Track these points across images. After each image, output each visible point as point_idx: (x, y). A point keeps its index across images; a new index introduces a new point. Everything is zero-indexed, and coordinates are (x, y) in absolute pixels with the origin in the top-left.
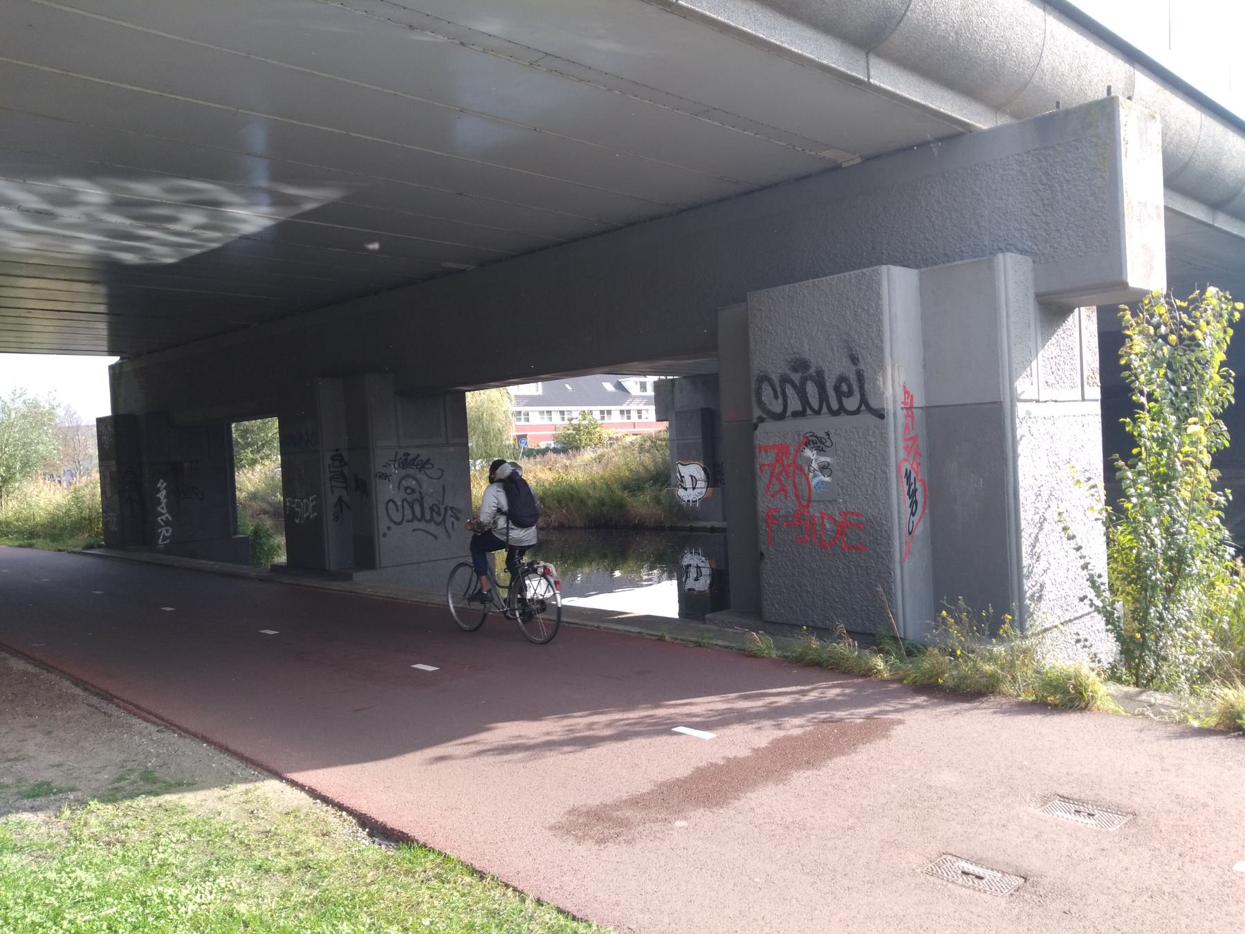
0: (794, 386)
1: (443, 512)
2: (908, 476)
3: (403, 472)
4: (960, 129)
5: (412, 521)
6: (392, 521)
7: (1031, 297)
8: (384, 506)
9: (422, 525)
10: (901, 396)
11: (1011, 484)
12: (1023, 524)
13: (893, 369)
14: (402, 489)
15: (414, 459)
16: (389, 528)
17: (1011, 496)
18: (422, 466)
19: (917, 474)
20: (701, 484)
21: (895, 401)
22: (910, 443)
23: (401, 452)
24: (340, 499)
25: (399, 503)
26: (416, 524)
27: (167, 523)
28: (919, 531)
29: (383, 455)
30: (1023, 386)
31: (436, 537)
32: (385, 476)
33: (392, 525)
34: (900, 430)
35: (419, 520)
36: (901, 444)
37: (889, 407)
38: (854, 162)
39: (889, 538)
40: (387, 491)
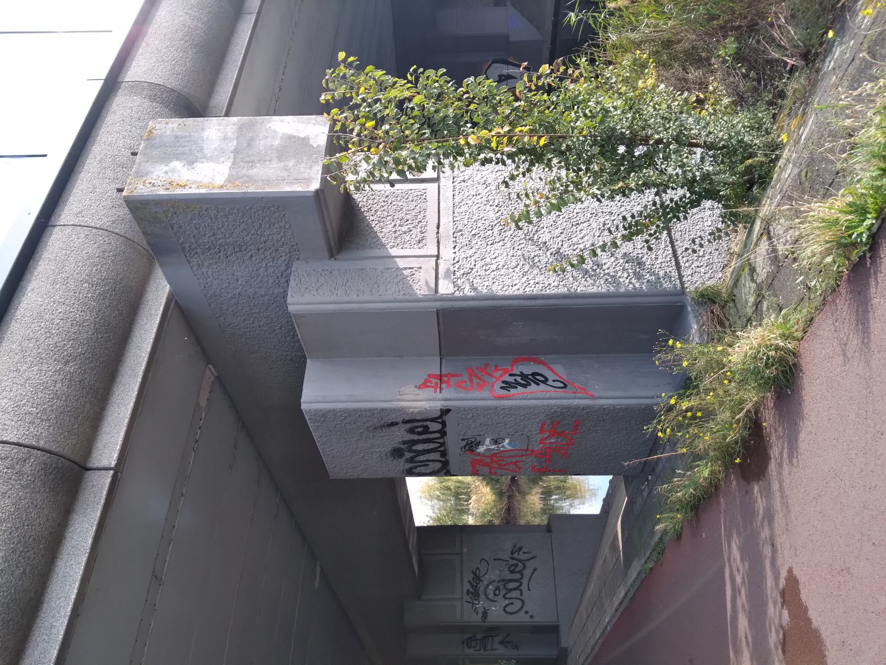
0: (416, 456)
1: (514, 562)
2: (508, 386)
3: (482, 596)
4: (173, 303)
5: (521, 591)
6: (520, 609)
7: (333, 264)
9: (525, 581)
10: (429, 393)
11: (522, 302)
12: (563, 290)
13: (402, 400)
15: (472, 585)
16: (527, 612)
17: (533, 302)
18: (478, 578)
21: (434, 400)
22: (475, 380)
23: (467, 598)
24: (501, 643)
25: (507, 602)
26: (524, 587)
28: (561, 371)
30: (421, 283)
31: (535, 570)
32: (485, 613)
33: (524, 610)
35: (521, 584)
36: (476, 394)
37: (438, 405)
38: (213, 369)
39: (569, 408)
40: (497, 613)
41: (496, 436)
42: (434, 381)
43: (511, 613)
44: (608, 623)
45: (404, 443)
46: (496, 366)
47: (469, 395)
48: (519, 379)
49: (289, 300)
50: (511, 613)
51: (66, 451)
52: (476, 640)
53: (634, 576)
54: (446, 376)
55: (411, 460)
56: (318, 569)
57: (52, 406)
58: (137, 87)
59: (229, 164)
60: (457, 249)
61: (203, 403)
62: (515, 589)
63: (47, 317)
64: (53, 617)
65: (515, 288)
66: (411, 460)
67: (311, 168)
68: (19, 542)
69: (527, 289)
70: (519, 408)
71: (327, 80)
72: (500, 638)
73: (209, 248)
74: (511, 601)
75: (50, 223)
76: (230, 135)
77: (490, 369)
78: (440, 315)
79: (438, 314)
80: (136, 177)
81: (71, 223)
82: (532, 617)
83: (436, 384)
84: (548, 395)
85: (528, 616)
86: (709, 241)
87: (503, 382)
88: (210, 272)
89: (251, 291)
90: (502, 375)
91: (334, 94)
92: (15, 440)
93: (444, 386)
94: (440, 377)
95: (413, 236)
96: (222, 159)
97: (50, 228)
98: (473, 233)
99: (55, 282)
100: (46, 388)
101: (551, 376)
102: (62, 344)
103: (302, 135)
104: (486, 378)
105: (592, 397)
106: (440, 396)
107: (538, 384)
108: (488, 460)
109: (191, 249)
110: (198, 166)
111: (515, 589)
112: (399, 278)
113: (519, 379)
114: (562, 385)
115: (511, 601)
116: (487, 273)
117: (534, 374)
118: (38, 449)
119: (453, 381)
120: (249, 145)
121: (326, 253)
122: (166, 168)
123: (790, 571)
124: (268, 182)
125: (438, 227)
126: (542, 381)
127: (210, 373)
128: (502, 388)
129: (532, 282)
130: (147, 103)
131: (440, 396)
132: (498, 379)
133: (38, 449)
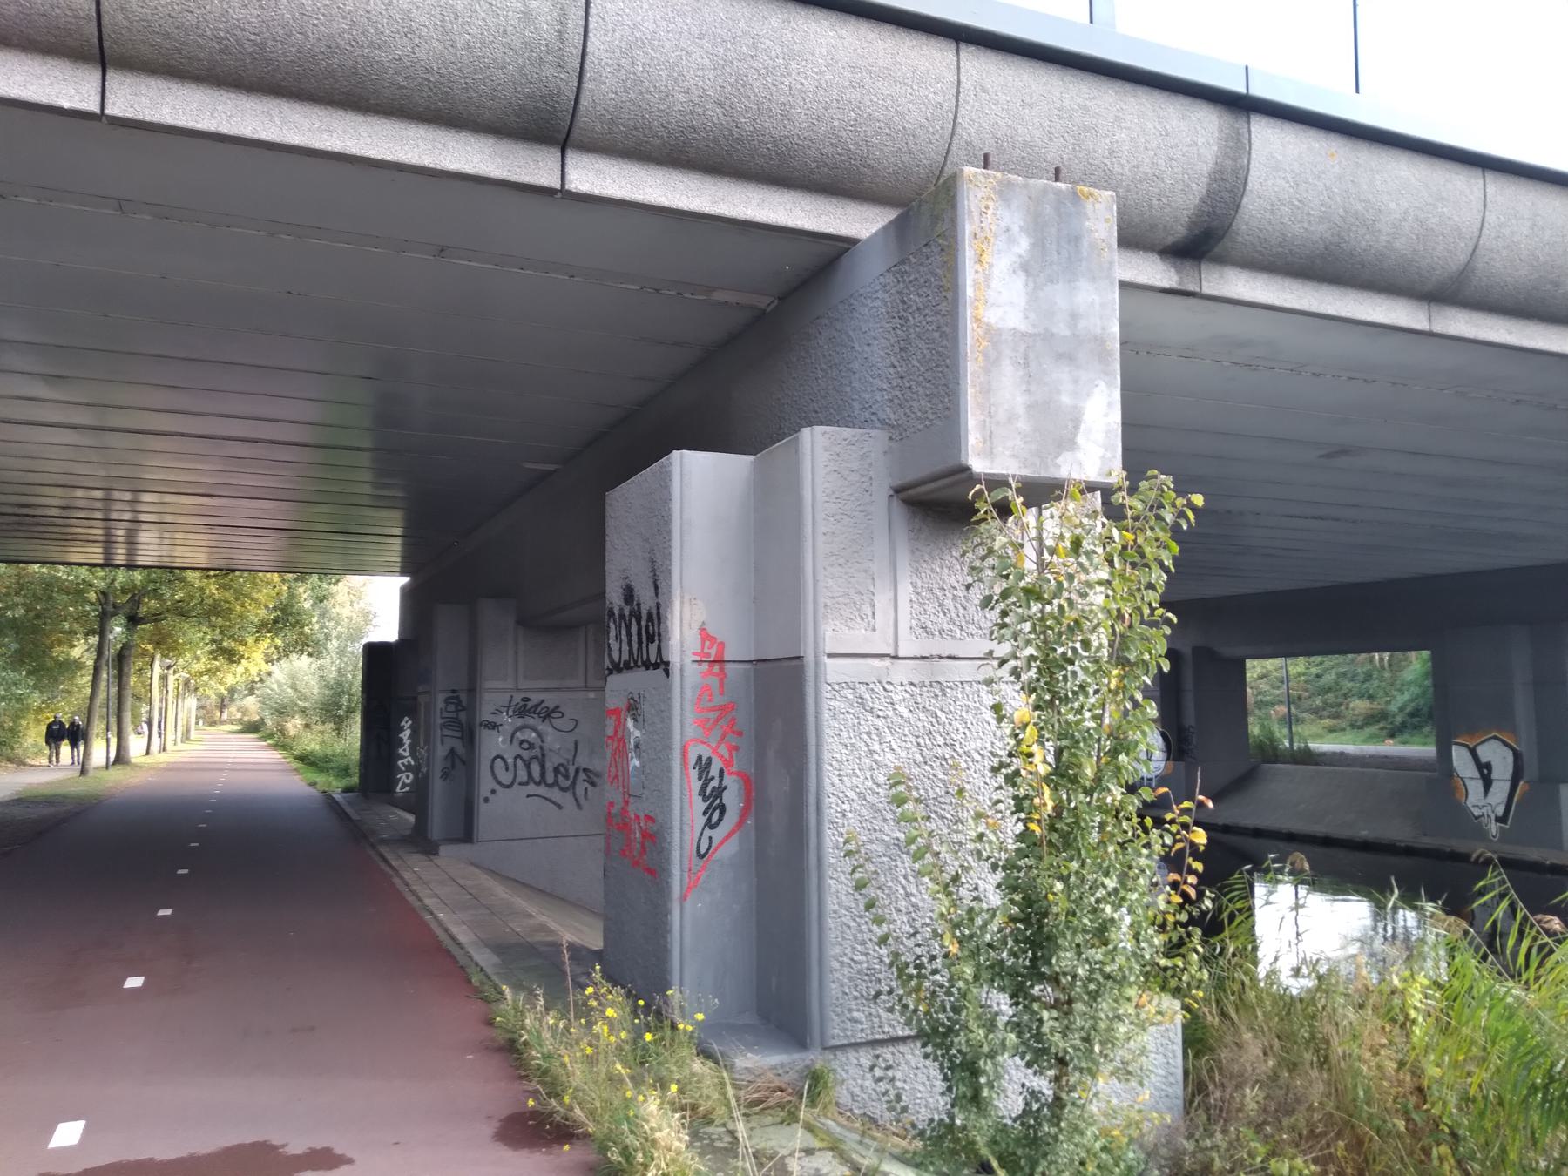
1: (572, 774)
2: (703, 766)
3: (520, 722)
5: (526, 784)
6: (499, 782)
7: (881, 492)
8: (488, 763)
9: (542, 790)
14: (516, 743)
15: (537, 706)
16: (493, 792)
17: (812, 808)
18: (547, 715)
19: (728, 763)
20: (1158, 754)
21: (683, 651)
23: (518, 697)
24: (452, 752)
25: (510, 761)
27: (408, 768)
29: (493, 699)
31: (560, 807)
32: (493, 726)
33: (498, 787)
34: (689, 694)
36: (690, 716)
39: (668, 860)
40: (494, 744)
41: (643, 747)
42: (713, 652)
43: (492, 767)
44: (436, 918)
45: (639, 605)
46: (736, 748)
47: (688, 707)
48: (714, 783)
49: (818, 429)
50: (492, 767)
51: (582, 119)
52: (457, 711)
53: (476, 957)
54: (722, 670)
55: (622, 616)
56: (552, 467)
57: (649, 92)
58: (1238, 148)
59: (1023, 326)
60: (908, 688)
61: (719, 296)
62: (530, 774)
63: (794, 65)
64: (345, 132)
65: (836, 780)
66: (622, 616)
67: (1013, 456)
68: (441, 75)
69: (833, 799)
70: (669, 781)
71: (1155, 477)
72: (461, 750)
73: (903, 302)
74: (511, 768)
75: (963, 46)
76: (1082, 324)
77: (732, 739)
78: (794, 663)
79: (798, 658)
80: (1000, 182)
81: (963, 79)
82: (486, 800)
83: (708, 655)
84: (687, 829)
85: (488, 794)
86: (886, 1093)
87: (709, 759)
88: (878, 303)
89: (856, 366)
90: (721, 756)
91: (1120, 489)
92: (589, 49)
93: (705, 666)
94: (720, 661)
95: (933, 618)
96: (1032, 316)
97: (954, 45)
98: (939, 713)
99: (853, 68)
100: (676, 80)
101: (718, 834)
102: (749, 92)
103: (1080, 439)
104: (716, 734)
105: (683, 898)
106: (688, 661)
107: (705, 813)
108: (620, 734)
109: (903, 273)
110: (1019, 282)
111: (530, 774)
112: (857, 598)
113: (714, 783)
114: (703, 851)
115: (511, 768)
116: (865, 736)
117: (722, 809)
118: (580, 82)
119: (714, 682)
120: (1060, 357)
121: (898, 483)
122: (1015, 229)
123: (350, 1161)
124: (986, 391)
125: (950, 657)
126: (710, 819)
127: (764, 302)
128: (700, 758)
129: (846, 806)
130: (1204, 168)
131: (688, 661)
132: (715, 751)
133: (580, 82)
